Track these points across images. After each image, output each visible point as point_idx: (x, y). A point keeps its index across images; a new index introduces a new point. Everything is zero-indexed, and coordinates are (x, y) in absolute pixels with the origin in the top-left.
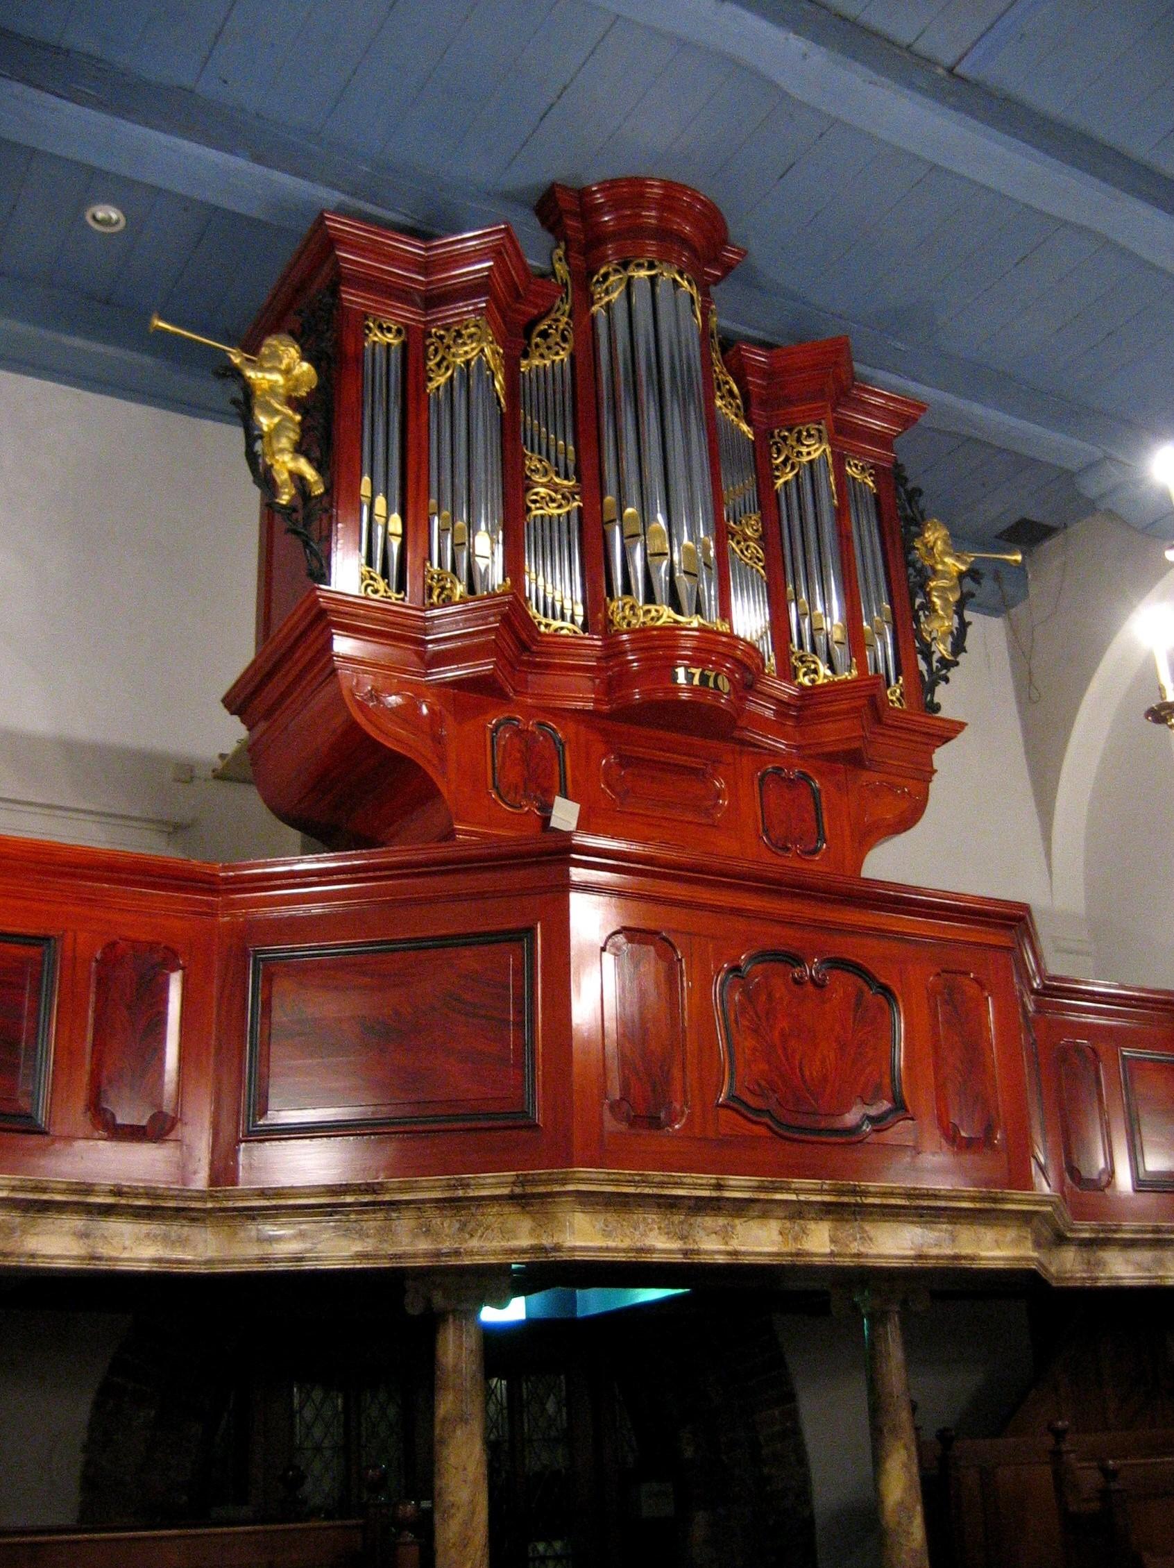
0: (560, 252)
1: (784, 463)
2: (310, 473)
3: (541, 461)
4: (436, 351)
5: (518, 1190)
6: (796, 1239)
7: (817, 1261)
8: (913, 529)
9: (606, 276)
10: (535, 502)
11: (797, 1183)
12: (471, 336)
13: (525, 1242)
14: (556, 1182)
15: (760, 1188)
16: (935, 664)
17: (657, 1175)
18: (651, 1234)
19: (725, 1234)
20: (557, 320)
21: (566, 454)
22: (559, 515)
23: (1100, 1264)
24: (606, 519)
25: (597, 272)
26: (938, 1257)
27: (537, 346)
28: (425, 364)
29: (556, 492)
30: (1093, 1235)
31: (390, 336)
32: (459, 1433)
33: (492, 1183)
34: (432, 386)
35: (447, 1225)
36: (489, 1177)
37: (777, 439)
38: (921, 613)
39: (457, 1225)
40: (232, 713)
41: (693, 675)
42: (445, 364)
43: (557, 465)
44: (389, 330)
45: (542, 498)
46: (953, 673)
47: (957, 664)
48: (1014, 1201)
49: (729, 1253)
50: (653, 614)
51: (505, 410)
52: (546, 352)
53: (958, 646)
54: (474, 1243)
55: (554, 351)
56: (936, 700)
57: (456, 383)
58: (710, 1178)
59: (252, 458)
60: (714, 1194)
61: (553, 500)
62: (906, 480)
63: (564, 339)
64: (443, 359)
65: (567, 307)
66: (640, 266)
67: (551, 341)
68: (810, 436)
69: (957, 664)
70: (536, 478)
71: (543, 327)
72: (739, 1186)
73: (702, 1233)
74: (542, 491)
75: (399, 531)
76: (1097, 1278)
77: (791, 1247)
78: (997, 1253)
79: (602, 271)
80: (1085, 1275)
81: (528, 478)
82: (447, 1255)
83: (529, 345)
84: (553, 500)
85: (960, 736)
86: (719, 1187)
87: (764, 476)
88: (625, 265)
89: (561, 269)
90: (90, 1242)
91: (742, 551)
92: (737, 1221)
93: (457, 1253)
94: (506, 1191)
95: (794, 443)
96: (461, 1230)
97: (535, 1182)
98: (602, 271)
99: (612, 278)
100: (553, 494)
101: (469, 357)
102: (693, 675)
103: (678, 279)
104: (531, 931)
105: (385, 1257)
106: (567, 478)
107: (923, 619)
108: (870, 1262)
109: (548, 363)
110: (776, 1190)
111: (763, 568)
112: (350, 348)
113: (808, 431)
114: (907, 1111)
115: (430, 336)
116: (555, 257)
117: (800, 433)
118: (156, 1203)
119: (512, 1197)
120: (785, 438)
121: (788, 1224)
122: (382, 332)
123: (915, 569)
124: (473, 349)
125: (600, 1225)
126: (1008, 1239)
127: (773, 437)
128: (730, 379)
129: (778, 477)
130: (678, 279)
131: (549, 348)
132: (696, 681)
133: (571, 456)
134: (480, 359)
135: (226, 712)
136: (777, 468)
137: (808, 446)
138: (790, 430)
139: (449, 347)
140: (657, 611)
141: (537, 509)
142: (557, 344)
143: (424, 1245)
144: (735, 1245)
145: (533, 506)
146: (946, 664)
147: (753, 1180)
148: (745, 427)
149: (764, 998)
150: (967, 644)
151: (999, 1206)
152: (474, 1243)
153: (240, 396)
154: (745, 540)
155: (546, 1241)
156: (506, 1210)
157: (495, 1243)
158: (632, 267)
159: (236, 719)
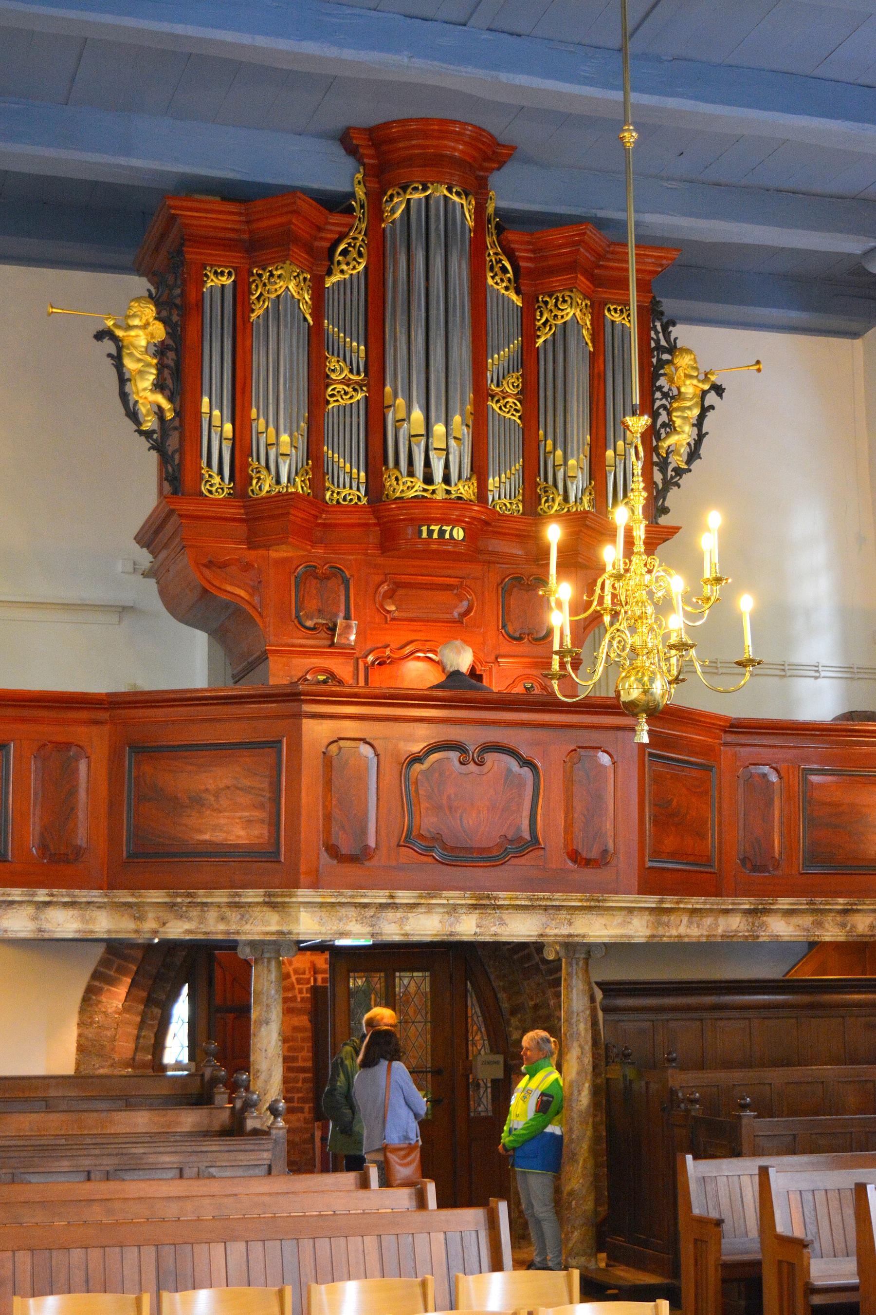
0: (359, 176)
1: (544, 324)
2: (166, 405)
3: (338, 361)
4: (257, 286)
5: (267, 900)
6: (451, 925)
7: (465, 939)
8: (666, 357)
9: (391, 197)
10: (332, 396)
11: (445, 894)
12: (279, 277)
13: (274, 928)
14: (286, 896)
15: (421, 897)
16: (670, 473)
17: (349, 892)
18: (351, 924)
19: (402, 922)
20: (355, 239)
21: (358, 352)
22: (351, 404)
23: (763, 925)
24: (385, 405)
25: (385, 194)
26: (556, 935)
27: (339, 263)
28: (250, 299)
29: (348, 386)
30: (752, 907)
31: (224, 279)
32: (263, 1029)
33: (252, 896)
34: (253, 316)
35: (234, 916)
36: (251, 892)
37: (541, 304)
38: (662, 431)
39: (239, 916)
40: (142, 547)
41: (433, 531)
42: (262, 299)
43: (351, 364)
44: (222, 273)
45: (339, 392)
46: (685, 480)
47: (690, 471)
48: (613, 901)
49: (403, 935)
50: (409, 484)
51: (311, 323)
52: (344, 267)
53: (694, 454)
54: (247, 927)
55: (351, 266)
56: (666, 504)
57: (270, 311)
58: (387, 893)
59: (124, 396)
60: (390, 901)
61: (346, 393)
62: (662, 313)
63: (360, 254)
64: (261, 294)
65: (364, 226)
66: (416, 189)
67: (349, 258)
68: (564, 301)
69: (690, 471)
70: (333, 376)
71: (342, 247)
72: (404, 896)
73: (385, 923)
74: (340, 387)
75: (230, 435)
76: (758, 937)
77: (448, 929)
78: (605, 932)
79: (389, 193)
80: (747, 934)
81: (328, 376)
82: (233, 933)
83: (332, 263)
84: (346, 393)
85: (676, 536)
86: (392, 897)
87: (529, 333)
88: (404, 189)
89: (360, 192)
90: (39, 922)
91: (500, 408)
92: (410, 915)
93: (238, 933)
94: (261, 900)
95: (553, 308)
96: (241, 919)
97: (274, 895)
98: (389, 193)
99: (396, 200)
100: (345, 388)
101: (279, 293)
102: (433, 531)
103: (449, 195)
104: (280, 742)
105: (201, 933)
106: (358, 374)
107: (663, 436)
108: (504, 939)
109: (347, 276)
110: (432, 898)
111: (520, 418)
112: (193, 296)
113: (563, 297)
114: (540, 844)
115: (253, 275)
116: (356, 182)
117: (557, 299)
118: (74, 900)
119: (265, 903)
120: (546, 303)
121: (446, 916)
122: (217, 277)
123: (662, 392)
124: (281, 287)
125: (317, 919)
126: (615, 923)
127: (538, 301)
128: (503, 257)
129: (539, 337)
130: (449, 195)
131: (348, 264)
132: (435, 536)
133: (362, 354)
134: (286, 295)
135: (138, 546)
136: (539, 329)
137: (562, 310)
138: (550, 296)
139: (265, 285)
140: (412, 482)
141: (335, 401)
142: (354, 259)
143: (222, 927)
144: (408, 928)
145: (331, 400)
146: (679, 472)
147: (415, 893)
148: (514, 297)
149: (437, 775)
150: (702, 451)
151: (601, 904)
152: (247, 927)
153: (114, 352)
154: (504, 398)
155: (285, 929)
156: (265, 909)
157: (259, 928)
158: (410, 190)
159: (145, 550)
